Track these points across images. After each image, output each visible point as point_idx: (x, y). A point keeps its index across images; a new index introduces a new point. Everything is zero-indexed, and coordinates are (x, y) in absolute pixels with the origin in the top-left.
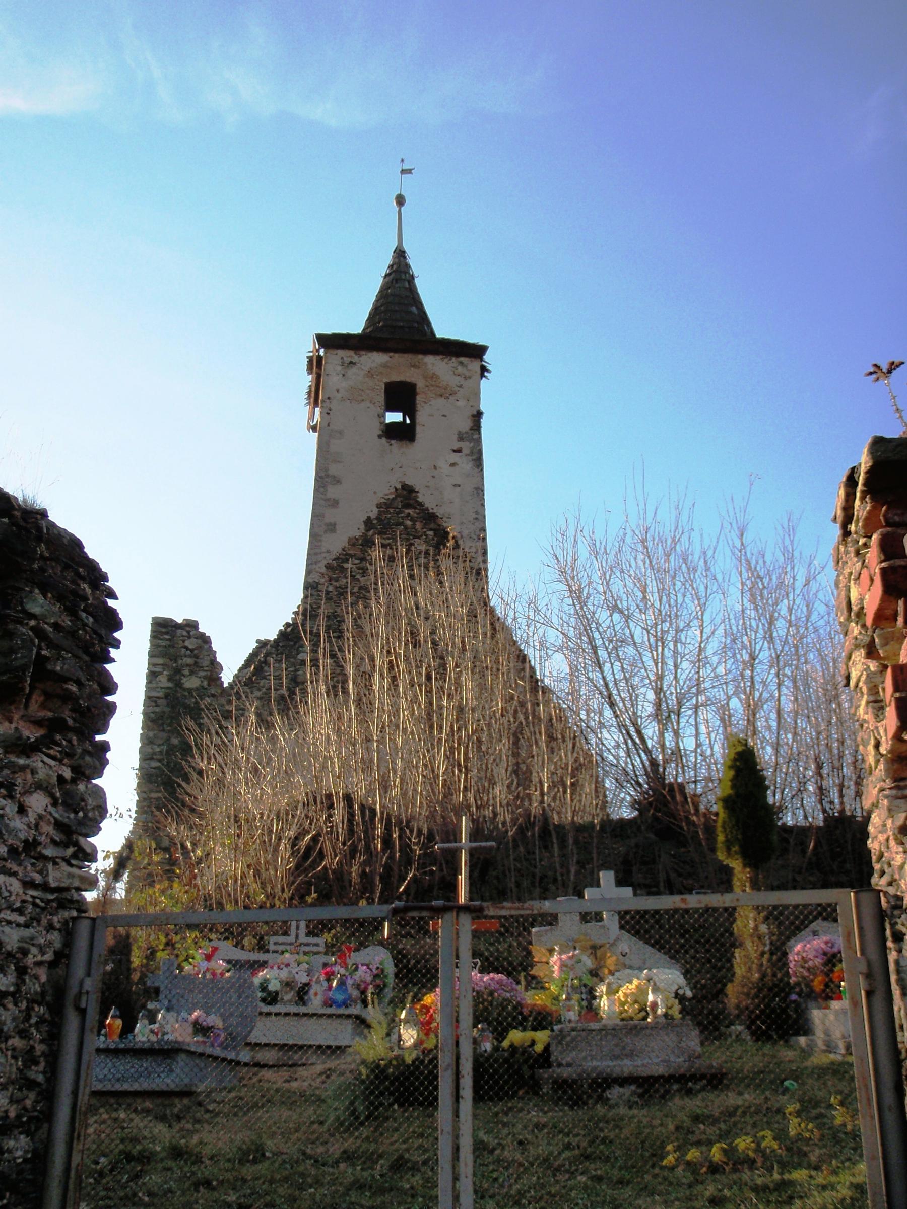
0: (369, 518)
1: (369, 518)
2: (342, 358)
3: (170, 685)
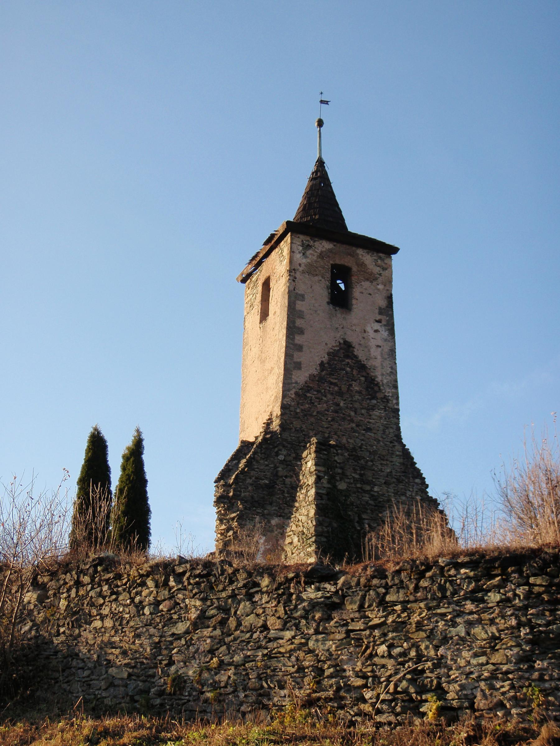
0: (322, 362)
1: (322, 362)
2: (302, 241)
3: (329, 486)
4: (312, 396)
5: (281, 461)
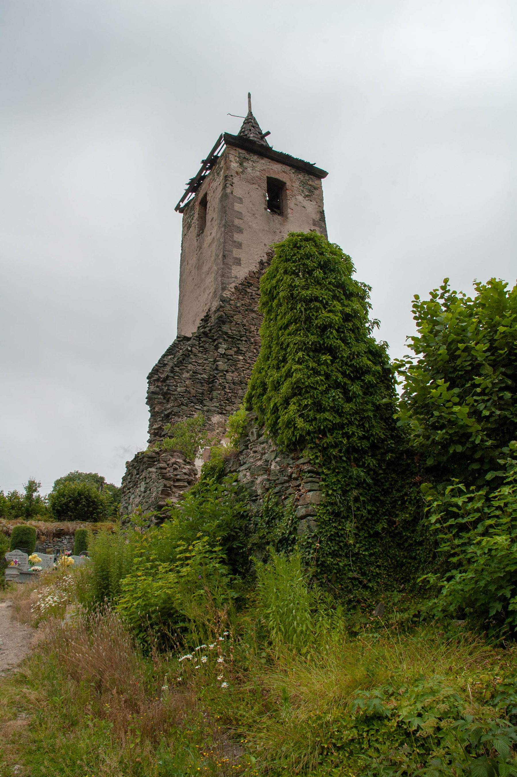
4: (252, 291)
5: (221, 354)
